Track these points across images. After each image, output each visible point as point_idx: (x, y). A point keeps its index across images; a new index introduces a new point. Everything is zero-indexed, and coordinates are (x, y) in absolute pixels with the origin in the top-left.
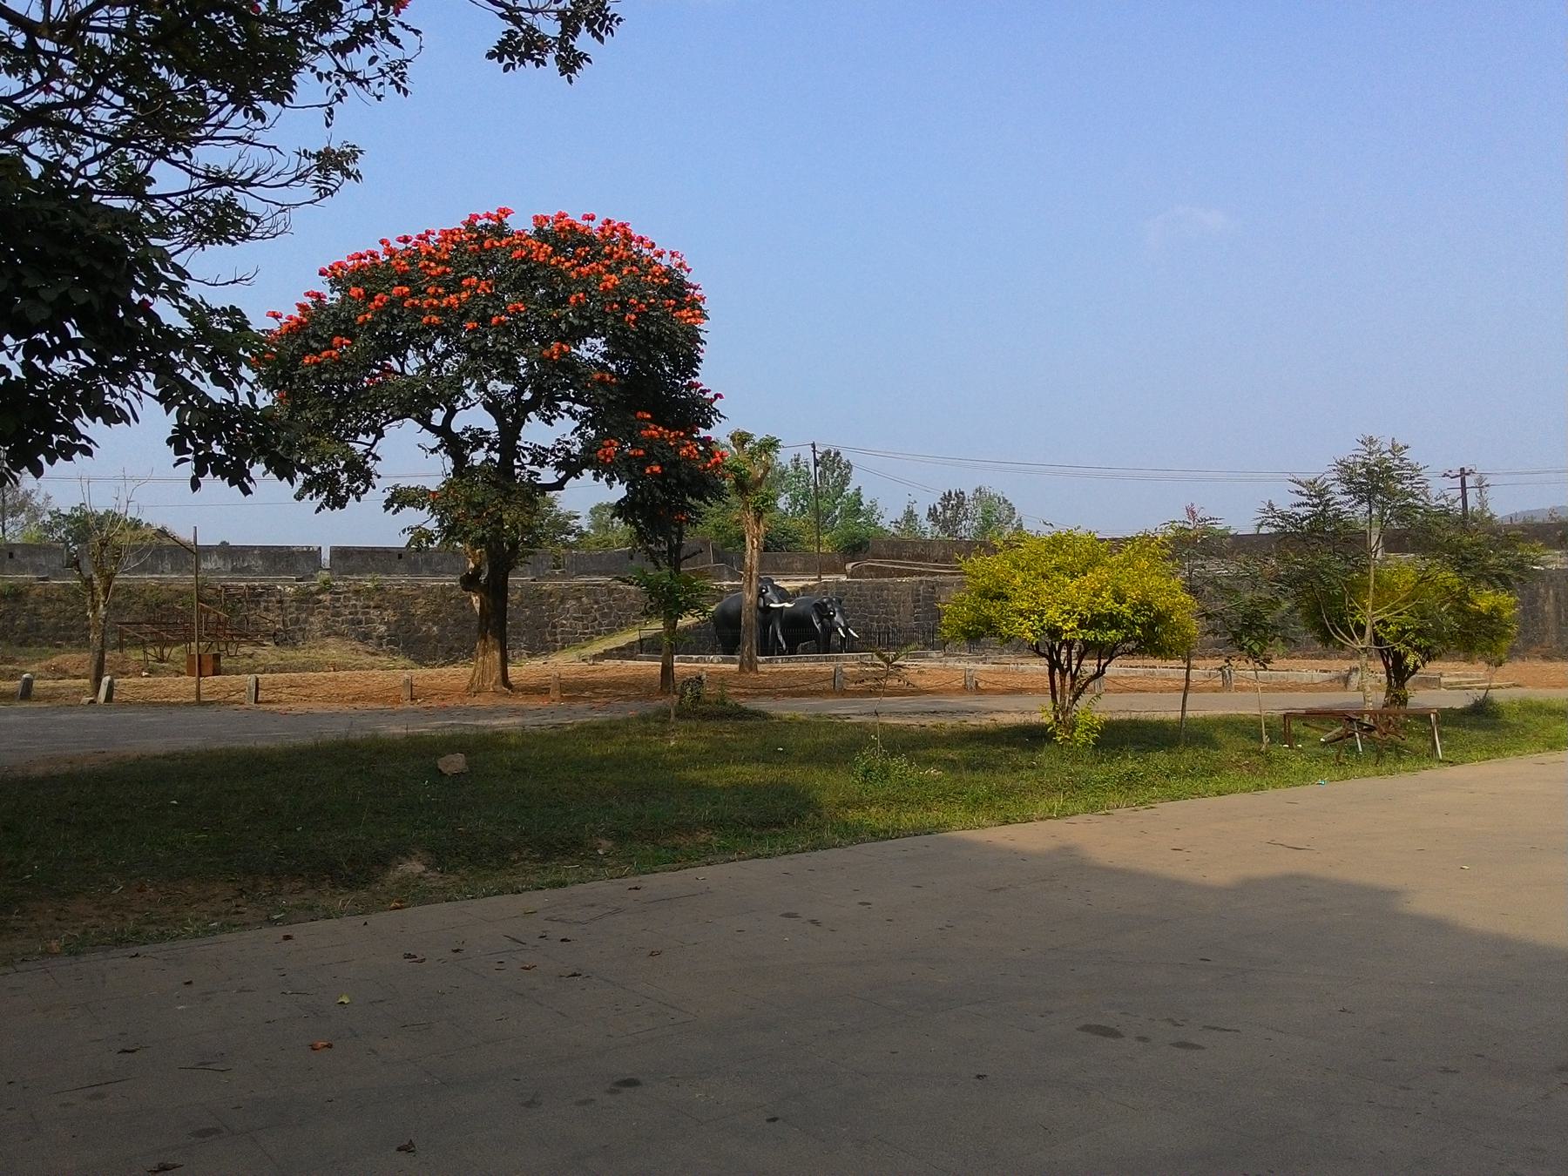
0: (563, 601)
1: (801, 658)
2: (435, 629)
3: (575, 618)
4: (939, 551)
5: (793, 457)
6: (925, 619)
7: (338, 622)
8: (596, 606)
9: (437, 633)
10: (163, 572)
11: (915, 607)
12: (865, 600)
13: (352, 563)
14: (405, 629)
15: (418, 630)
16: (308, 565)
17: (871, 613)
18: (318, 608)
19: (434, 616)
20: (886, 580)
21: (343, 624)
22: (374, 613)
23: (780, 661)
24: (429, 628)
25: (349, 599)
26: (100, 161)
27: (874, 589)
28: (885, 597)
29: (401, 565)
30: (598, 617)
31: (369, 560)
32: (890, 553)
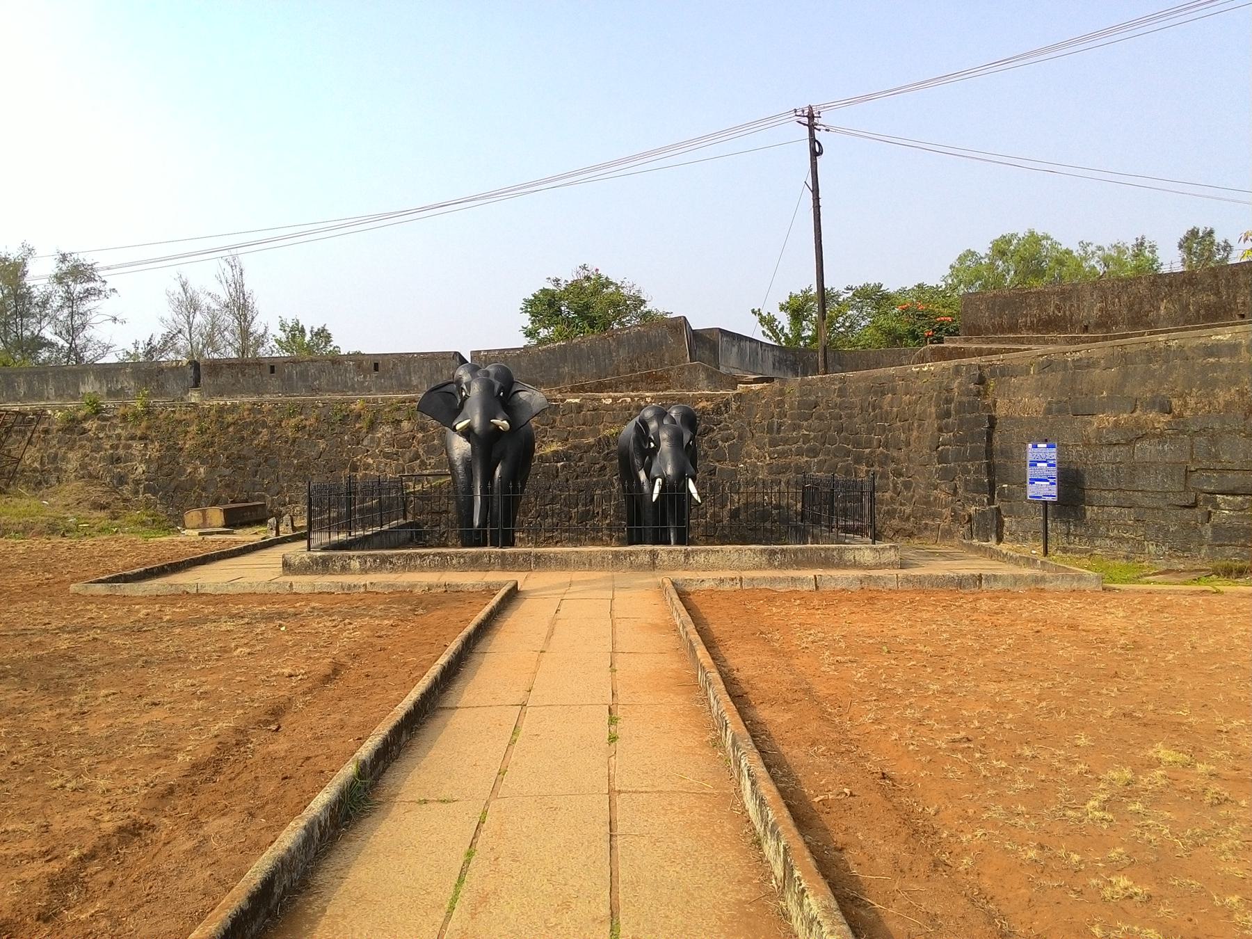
0: (372, 426)
1: (421, 556)
2: (202, 470)
3: (387, 456)
4: (1092, 306)
5: (1135, 242)
6: (959, 457)
7: (95, 459)
8: (420, 435)
9: (203, 476)
10: (48, 398)
11: (940, 430)
12: (850, 417)
13: (222, 380)
14: (166, 470)
15: (182, 471)
16: (177, 384)
17: (857, 444)
18: (80, 440)
19: (204, 452)
20: (891, 370)
21: (100, 462)
22: (137, 446)
23: (355, 564)
24: (196, 469)
25: (115, 426)
26: (1223, 260)
27: (870, 390)
28: (886, 407)
29: (274, 381)
30: (421, 452)
31: (240, 375)
32: (997, 320)
